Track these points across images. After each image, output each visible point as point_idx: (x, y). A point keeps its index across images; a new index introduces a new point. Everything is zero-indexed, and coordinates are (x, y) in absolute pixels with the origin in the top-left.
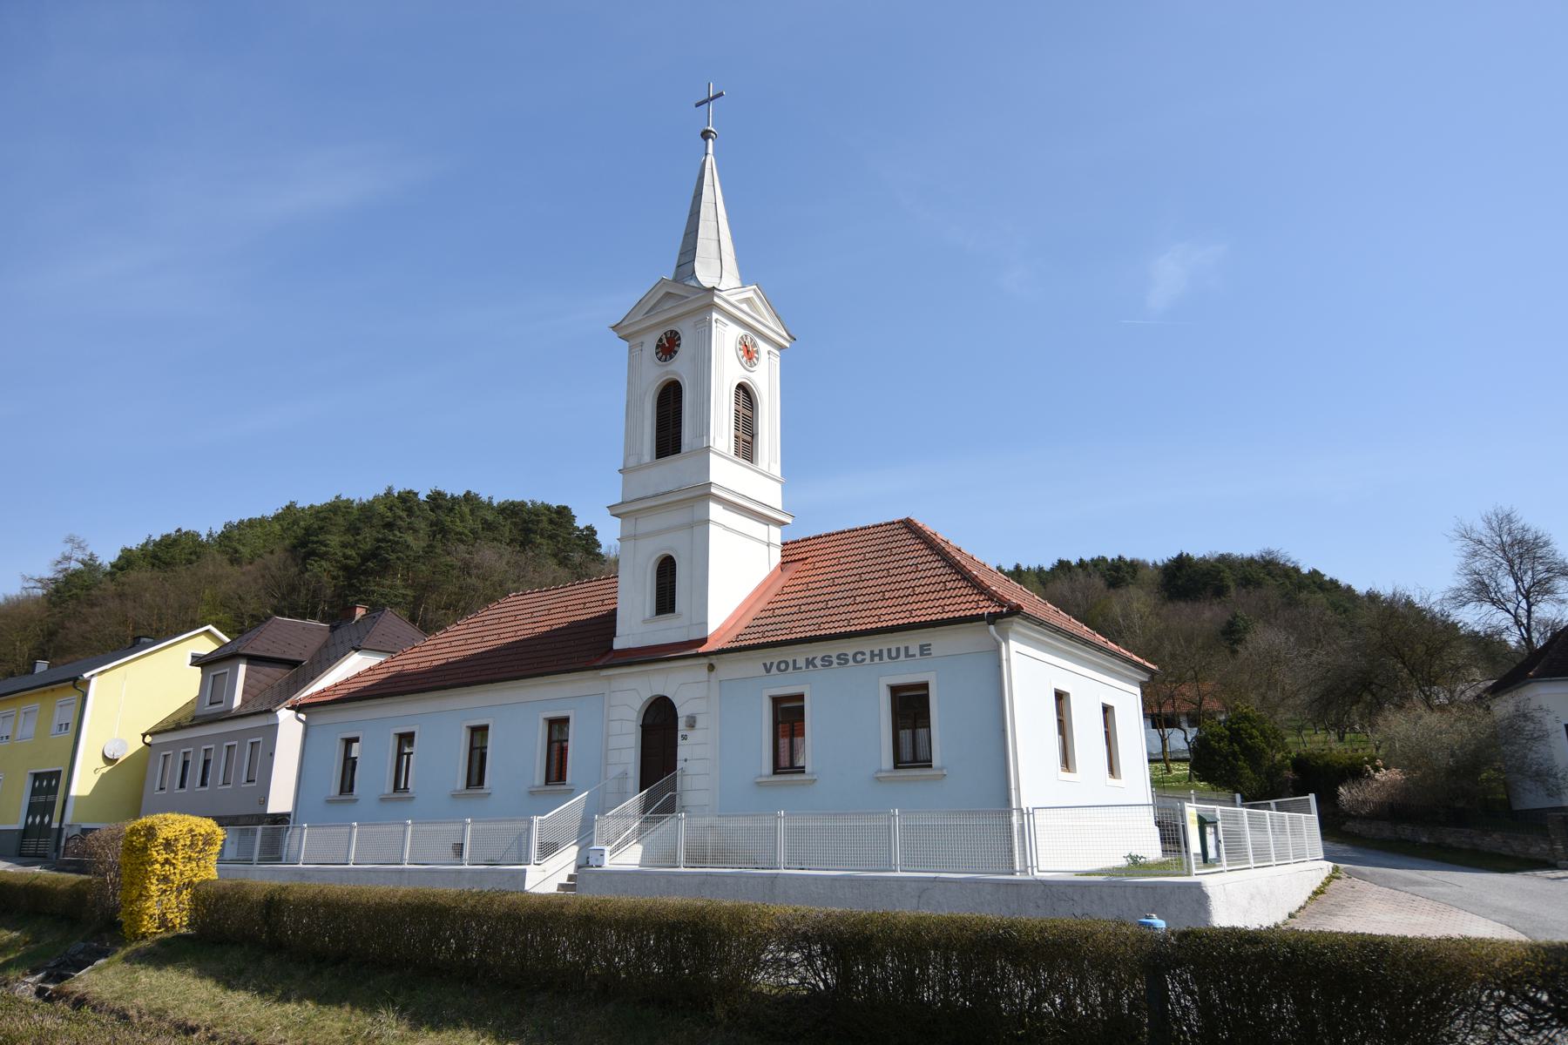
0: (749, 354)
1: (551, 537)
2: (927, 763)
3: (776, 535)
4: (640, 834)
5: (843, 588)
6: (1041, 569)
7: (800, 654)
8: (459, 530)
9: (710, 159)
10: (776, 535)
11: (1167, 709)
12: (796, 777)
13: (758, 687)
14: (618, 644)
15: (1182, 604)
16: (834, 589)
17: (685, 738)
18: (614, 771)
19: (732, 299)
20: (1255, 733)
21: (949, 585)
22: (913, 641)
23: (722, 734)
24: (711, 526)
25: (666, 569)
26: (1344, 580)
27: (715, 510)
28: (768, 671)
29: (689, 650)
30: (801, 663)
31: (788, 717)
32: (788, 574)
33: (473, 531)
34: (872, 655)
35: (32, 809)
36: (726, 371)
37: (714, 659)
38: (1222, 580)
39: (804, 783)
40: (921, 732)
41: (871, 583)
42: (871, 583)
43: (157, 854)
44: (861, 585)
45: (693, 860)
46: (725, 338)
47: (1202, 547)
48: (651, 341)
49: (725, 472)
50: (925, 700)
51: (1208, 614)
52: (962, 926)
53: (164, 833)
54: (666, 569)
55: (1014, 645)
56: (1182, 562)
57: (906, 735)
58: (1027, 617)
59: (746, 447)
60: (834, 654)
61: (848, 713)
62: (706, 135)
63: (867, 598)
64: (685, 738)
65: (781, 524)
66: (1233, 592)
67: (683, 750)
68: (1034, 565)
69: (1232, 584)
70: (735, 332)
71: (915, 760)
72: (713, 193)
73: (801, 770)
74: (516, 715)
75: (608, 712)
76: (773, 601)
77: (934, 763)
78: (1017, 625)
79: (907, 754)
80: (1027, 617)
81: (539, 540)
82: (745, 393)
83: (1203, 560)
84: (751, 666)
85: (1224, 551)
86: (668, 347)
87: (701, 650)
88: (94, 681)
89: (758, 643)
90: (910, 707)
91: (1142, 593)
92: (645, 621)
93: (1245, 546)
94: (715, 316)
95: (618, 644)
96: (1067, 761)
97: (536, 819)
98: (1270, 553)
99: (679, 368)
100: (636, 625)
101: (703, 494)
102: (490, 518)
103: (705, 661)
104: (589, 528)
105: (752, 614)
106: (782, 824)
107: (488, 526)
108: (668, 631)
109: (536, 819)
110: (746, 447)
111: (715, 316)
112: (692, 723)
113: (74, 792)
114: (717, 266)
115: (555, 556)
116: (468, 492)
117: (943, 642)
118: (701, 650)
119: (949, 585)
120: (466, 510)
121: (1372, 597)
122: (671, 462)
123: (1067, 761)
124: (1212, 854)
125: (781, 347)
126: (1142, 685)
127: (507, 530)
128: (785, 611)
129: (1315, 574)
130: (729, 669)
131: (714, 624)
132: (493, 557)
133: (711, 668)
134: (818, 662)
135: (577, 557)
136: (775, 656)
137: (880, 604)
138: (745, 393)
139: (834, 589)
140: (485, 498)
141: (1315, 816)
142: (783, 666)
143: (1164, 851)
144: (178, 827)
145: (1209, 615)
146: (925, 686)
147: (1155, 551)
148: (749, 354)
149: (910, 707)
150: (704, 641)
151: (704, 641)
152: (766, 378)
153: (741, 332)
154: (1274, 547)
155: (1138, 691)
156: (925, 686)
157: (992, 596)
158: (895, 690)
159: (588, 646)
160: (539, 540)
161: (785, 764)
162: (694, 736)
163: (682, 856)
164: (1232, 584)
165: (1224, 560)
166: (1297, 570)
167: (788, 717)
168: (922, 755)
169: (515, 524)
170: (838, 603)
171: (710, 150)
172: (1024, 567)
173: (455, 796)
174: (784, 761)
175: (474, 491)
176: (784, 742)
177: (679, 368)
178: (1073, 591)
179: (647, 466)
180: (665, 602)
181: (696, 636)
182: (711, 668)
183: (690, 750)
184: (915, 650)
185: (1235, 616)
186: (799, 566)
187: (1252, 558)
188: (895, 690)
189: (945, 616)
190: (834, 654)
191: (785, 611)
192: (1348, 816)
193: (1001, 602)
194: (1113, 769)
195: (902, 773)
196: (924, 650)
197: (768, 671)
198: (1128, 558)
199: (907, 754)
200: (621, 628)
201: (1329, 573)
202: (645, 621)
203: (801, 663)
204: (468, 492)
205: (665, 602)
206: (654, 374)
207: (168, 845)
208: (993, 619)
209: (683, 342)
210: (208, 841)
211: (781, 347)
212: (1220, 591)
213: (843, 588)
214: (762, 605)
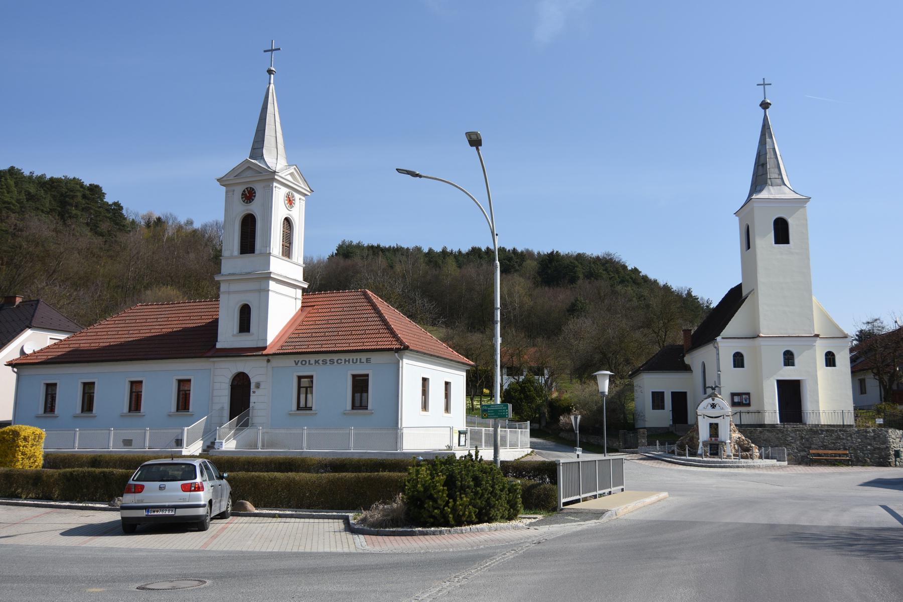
0: (290, 201)
2: (366, 408)
4: (235, 436)
5: (333, 326)
6: (460, 252)
7: (312, 358)
9: (272, 86)
11: (516, 363)
12: (308, 412)
13: (290, 371)
14: (218, 346)
15: (547, 288)
16: (329, 326)
17: (254, 392)
18: (217, 407)
19: (283, 176)
20: (532, 388)
21: (381, 331)
22: (364, 357)
23: (271, 393)
24: (270, 293)
25: (245, 312)
26: (652, 276)
27: (272, 285)
28: (297, 364)
29: (258, 351)
30: (312, 362)
31: (305, 385)
32: (305, 314)
34: (345, 361)
35: (711, 436)
36: (279, 211)
37: (270, 357)
38: (575, 273)
39: (311, 414)
40: (365, 395)
41: (346, 325)
42: (346, 325)
43: (21, 443)
44: (342, 325)
45: (263, 446)
46: (279, 194)
47: (567, 247)
48: (239, 190)
49: (278, 266)
50: (367, 381)
51: (561, 297)
52: (371, 460)
53: (23, 434)
54: (245, 312)
55: (405, 361)
56: (553, 257)
57: (358, 395)
58: (411, 350)
59: (287, 251)
60: (328, 359)
61: (333, 385)
63: (344, 333)
64: (254, 392)
66: (580, 282)
67: (253, 398)
68: (455, 250)
69: (581, 276)
70: (283, 191)
71: (361, 406)
72: (273, 109)
73: (310, 409)
74: (159, 378)
75: (212, 380)
76: (297, 328)
77: (370, 407)
78: (407, 353)
79: (357, 404)
80: (411, 350)
81: (74, 211)
82: (288, 222)
83: (568, 256)
84: (289, 361)
85: (581, 252)
86: (249, 196)
87: (264, 352)
89: (294, 349)
90: (360, 384)
91: (522, 280)
92: (234, 335)
93: (594, 249)
94: (275, 184)
95: (218, 346)
96: (425, 407)
97: (186, 429)
98: (609, 255)
99: (254, 208)
100: (228, 334)
101: (268, 277)
102: (32, 190)
103: (266, 358)
104: (117, 204)
105: (287, 335)
106: (305, 432)
107: (30, 197)
108: (245, 341)
109: (186, 429)
110: (287, 251)
111: (275, 184)
112: (258, 386)
114: (275, 157)
115: (87, 224)
117: (376, 358)
118: (264, 352)
119: (381, 331)
120: (11, 182)
121: (666, 288)
122: (248, 257)
123: (425, 407)
124: (462, 443)
125: (305, 195)
126: (468, 372)
127: (48, 201)
128: (305, 335)
129: (635, 271)
130: (275, 362)
131: (270, 341)
132: (41, 226)
133: (268, 361)
134: (320, 362)
135: (104, 226)
136: (300, 358)
137: (350, 337)
138: (288, 222)
139: (329, 326)
140: (27, 173)
141: (528, 430)
142: (304, 363)
144: (29, 431)
145: (561, 297)
146: (367, 375)
147: (542, 246)
148: (290, 201)
149: (360, 384)
150: (265, 348)
151: (265, 348)
152: (298, 215)
154: (612, 251)
155: (465, 374)
156: (367, 375)
157: (398, 340)
158: (354, 376)
159: (200, 342)
160: (74, 211)
161: (303, 407)
162: (258, 392)
163: (260, 445)
164: (581, 276)
165: (580, 257)
166: (624, 267)
167: (305, 385)
168: (364, 404)
169: (54, 197)
170: (331, 334)
172: (449, 250)
173: (123, 416)
174: (302, 404)
175: (17, 166)
176: (303, 397)
177: (254, 208)
178: (478, 275)
179: (236, 257)
180: (245, 325)
181: (261, 345)
182: (268, 361)
183: (255, 398)
184: (364, 360)
185: (577, 300)
186: (310, 308)
187: (598, 257)
188: (354, 376)
189: (378, 347)
190: (328, 359)
191: (305, 335)
192: (562, 430)
193: (402, 343)
194: (447, 409)
195: (355, 411)
196: (368, 360)
197: (297, 364)
198: (519, 249)
199: (357, 404)
200: (220, 337)
201: (644, 271)
202: (234, 335)
203: (312, 362)
205: (245, 325)
206: (241, 210)
207: (25, 439)
208: (397, 350)
209: (257, 195)
210: (40, 437)
212: (573, 280)
213: (333, 326)
214: (291, 330)
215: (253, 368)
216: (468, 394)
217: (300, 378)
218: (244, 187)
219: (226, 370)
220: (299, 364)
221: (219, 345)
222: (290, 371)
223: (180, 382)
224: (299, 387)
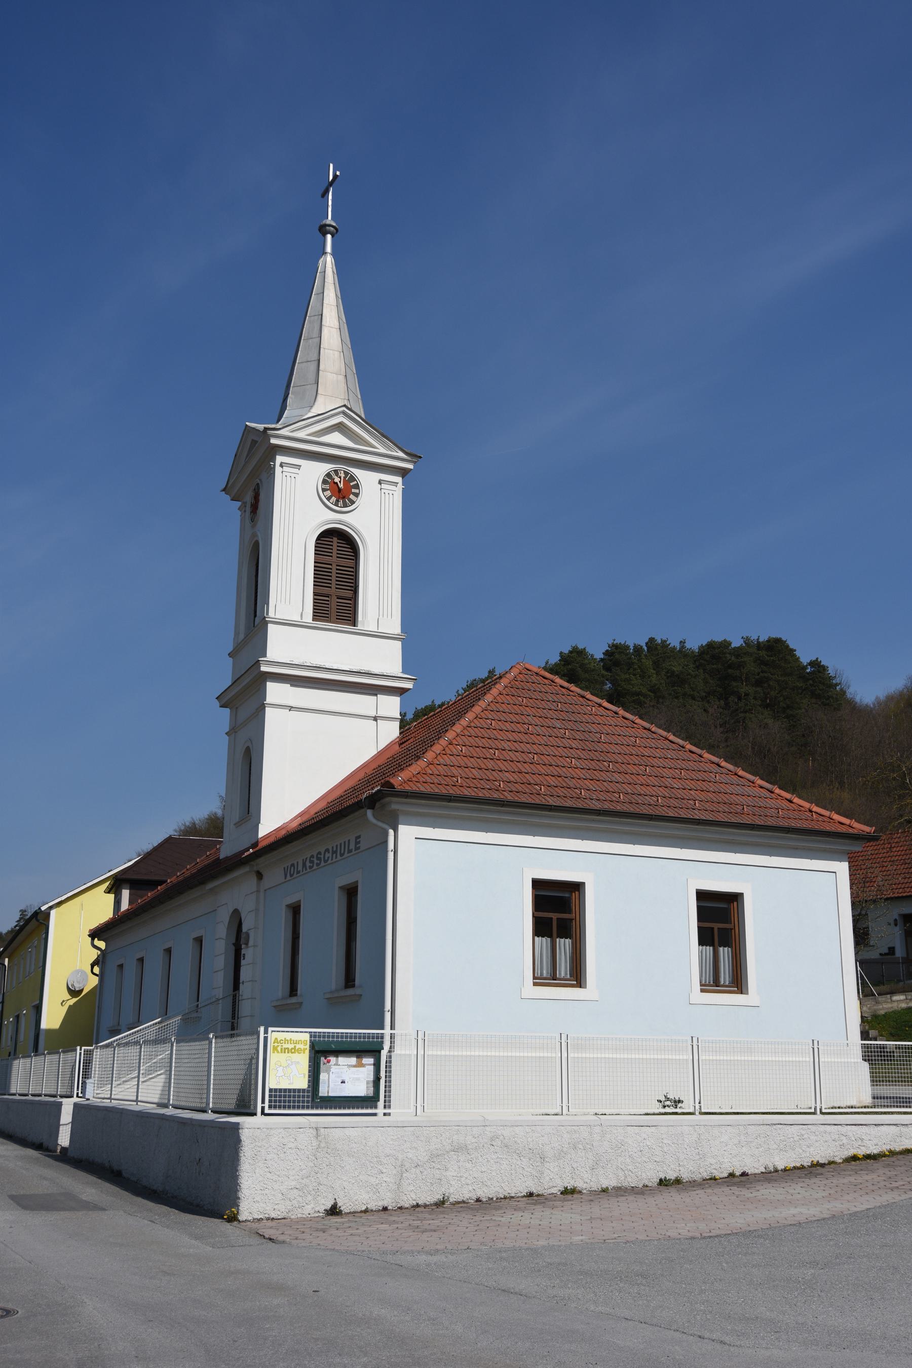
1: (759, 683)
3: (391, 706)
8: (636, 689)
10: (391, 706)
33: (654, 690)
62: (323, 230)
65: (400, 692)
81: (744, 689)
88: (53, 913)
104: (815, 664)
107: (676, 680)
113: (44, 1025)
116: (652, 640)
120: (648, 663)
125: (403, 472)
133: (260, 875)
140: (674, 643)
143: (876, 1080)
148: (341, 492)
152: (378, 518)
153: (325, 468)
171: (329, 249)
204: (652, 640)
211: (403, 472)
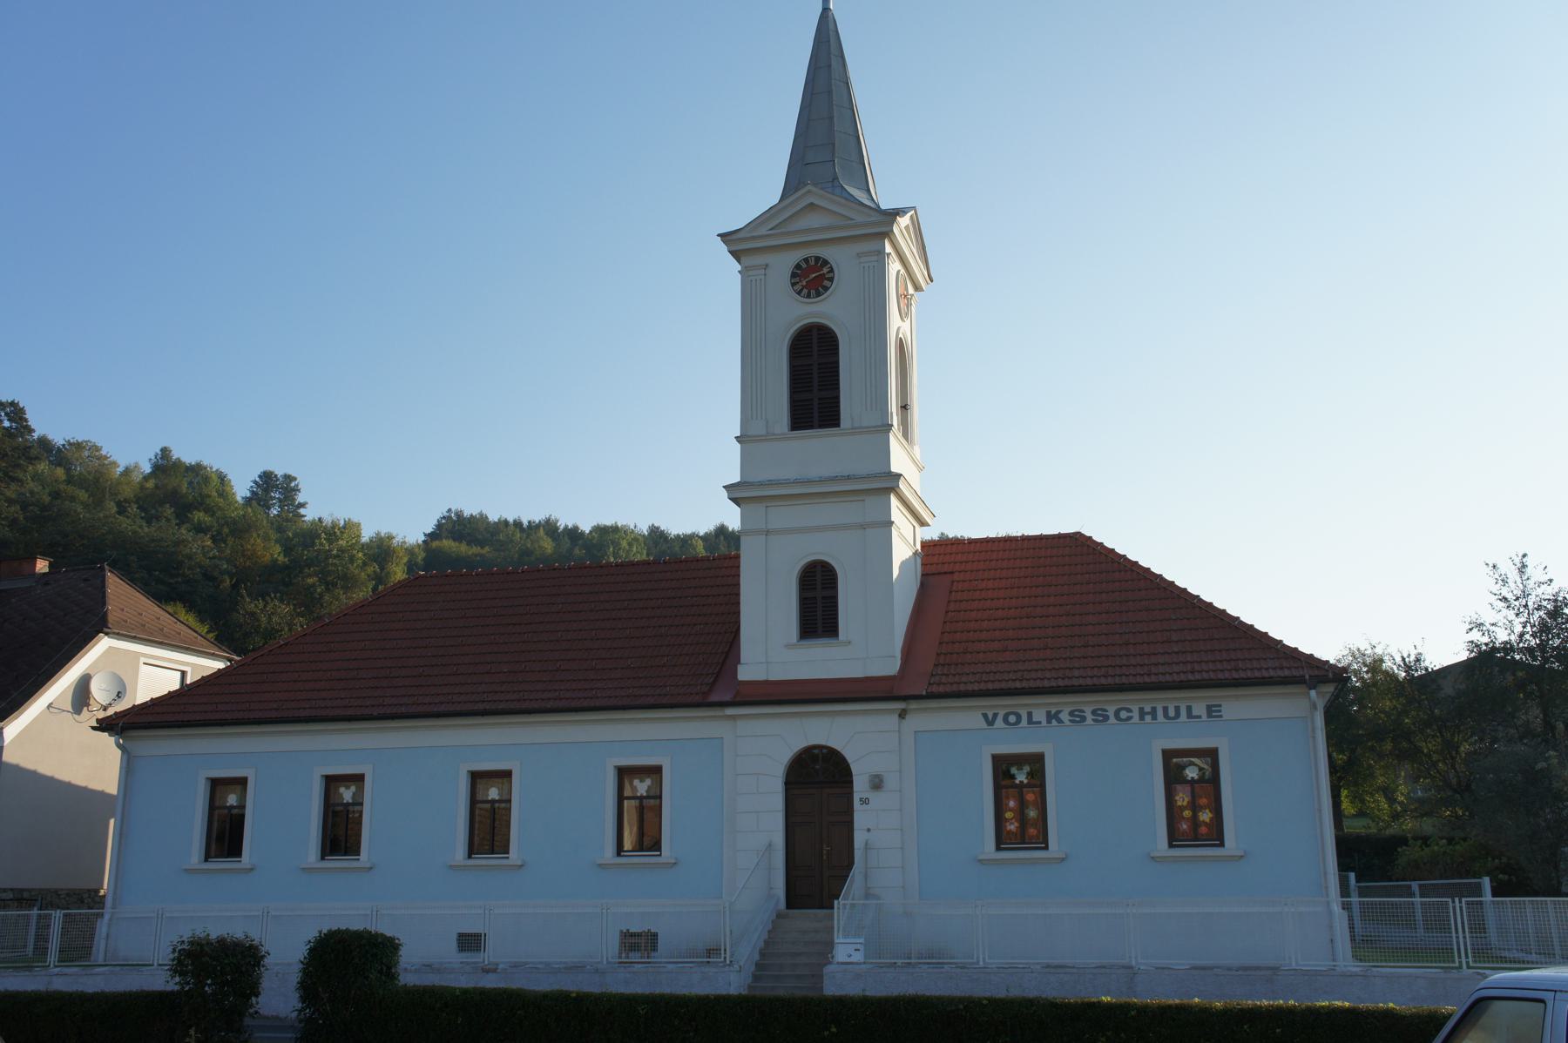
17: (865, 801)
28: (990, 723)
34: (1142, 714)
48: (785, 263)
86: (812, 277)
92: (789, 646)
133: (902, 714)
134: (1065, 716)
162: (876, 799)
177: (830, 310)
197: (990, 723)
198: (328, 520)
215: (859, 737)
216: (243, 816)
217: (624, 773)
218: (796, 257)
219: (764, 748)
220: (999, 722)
221: (745, 673)
222: (967, 738)
223: (216, 785)
224: (621, 799)
